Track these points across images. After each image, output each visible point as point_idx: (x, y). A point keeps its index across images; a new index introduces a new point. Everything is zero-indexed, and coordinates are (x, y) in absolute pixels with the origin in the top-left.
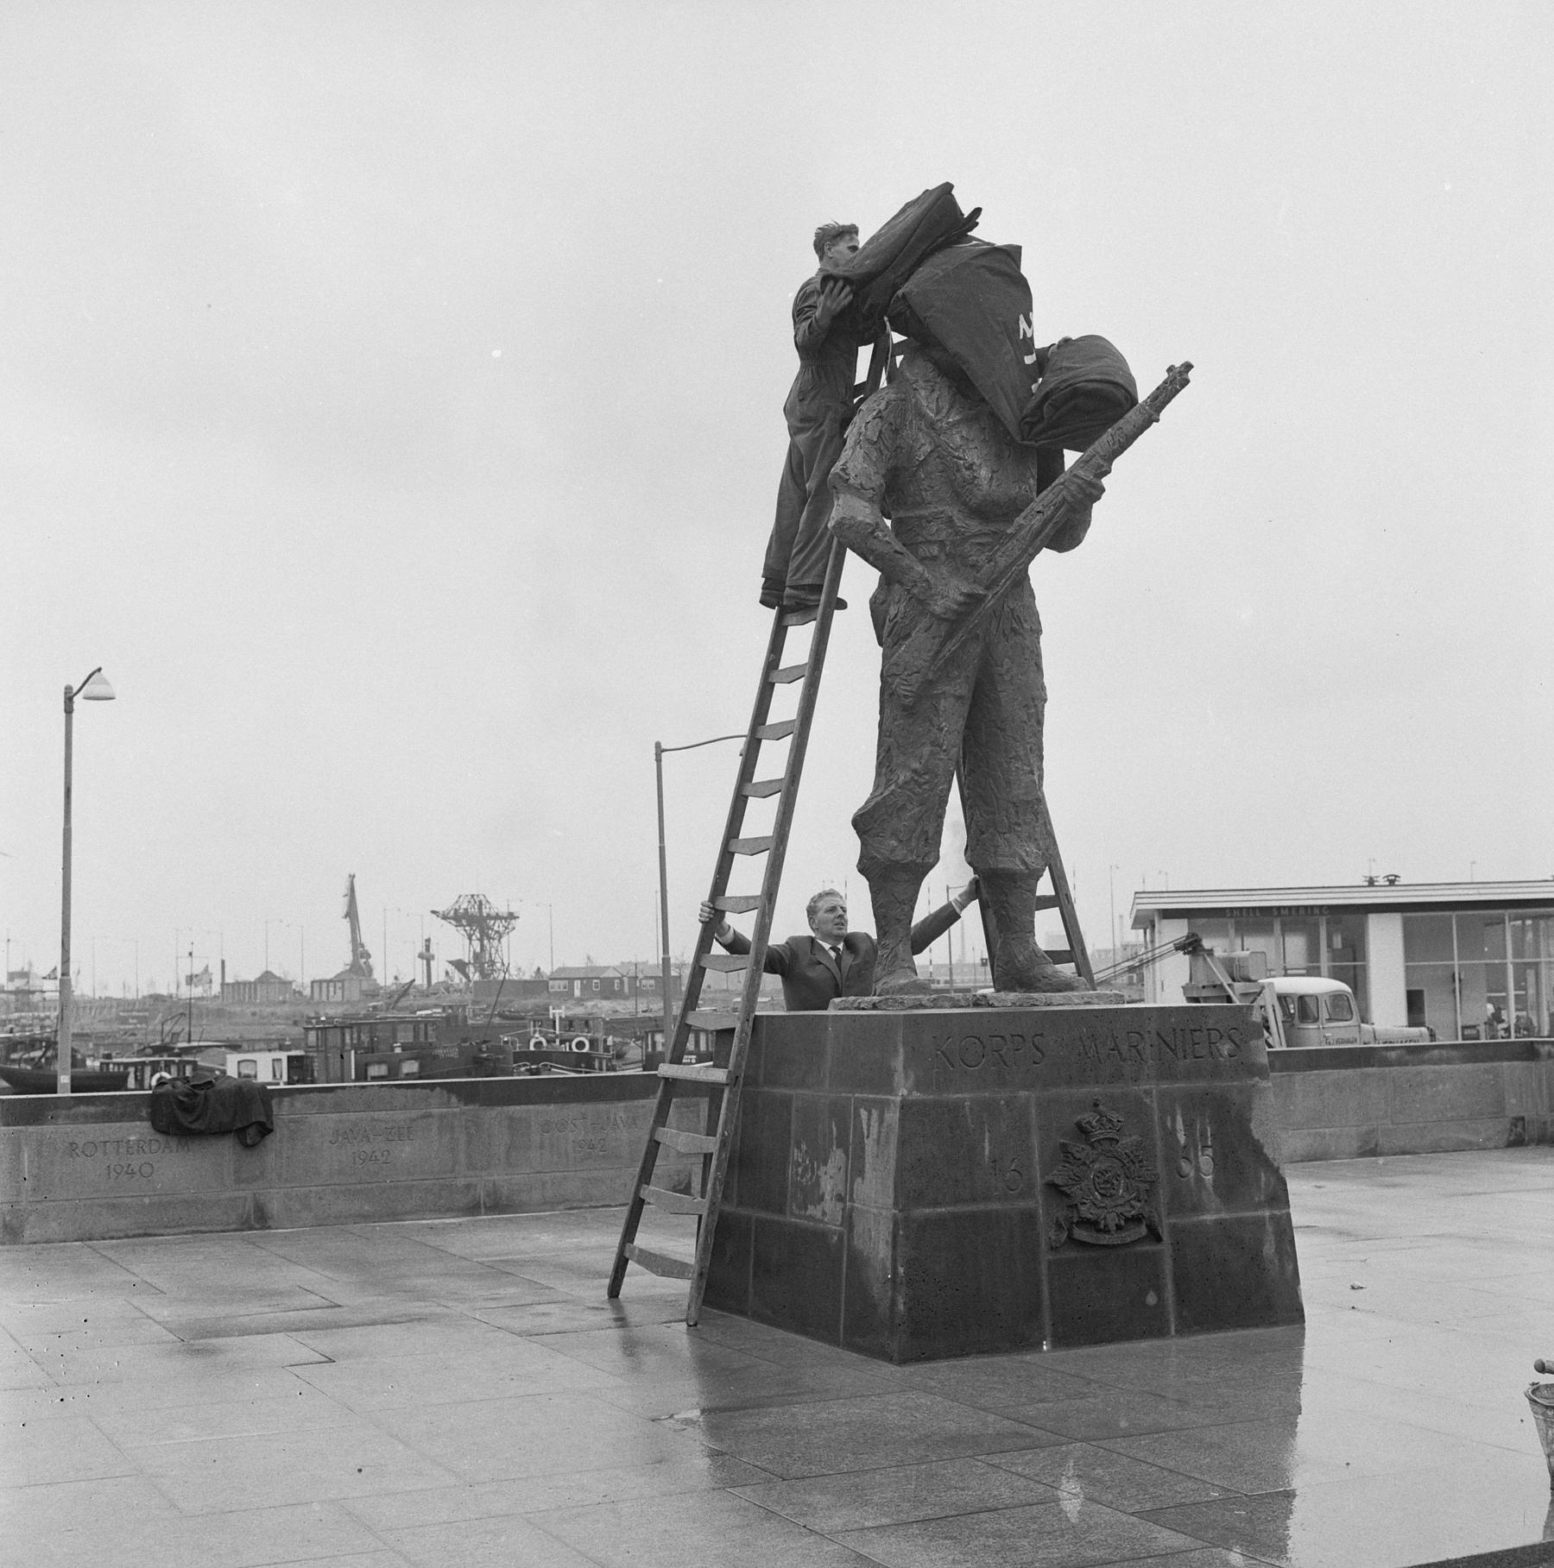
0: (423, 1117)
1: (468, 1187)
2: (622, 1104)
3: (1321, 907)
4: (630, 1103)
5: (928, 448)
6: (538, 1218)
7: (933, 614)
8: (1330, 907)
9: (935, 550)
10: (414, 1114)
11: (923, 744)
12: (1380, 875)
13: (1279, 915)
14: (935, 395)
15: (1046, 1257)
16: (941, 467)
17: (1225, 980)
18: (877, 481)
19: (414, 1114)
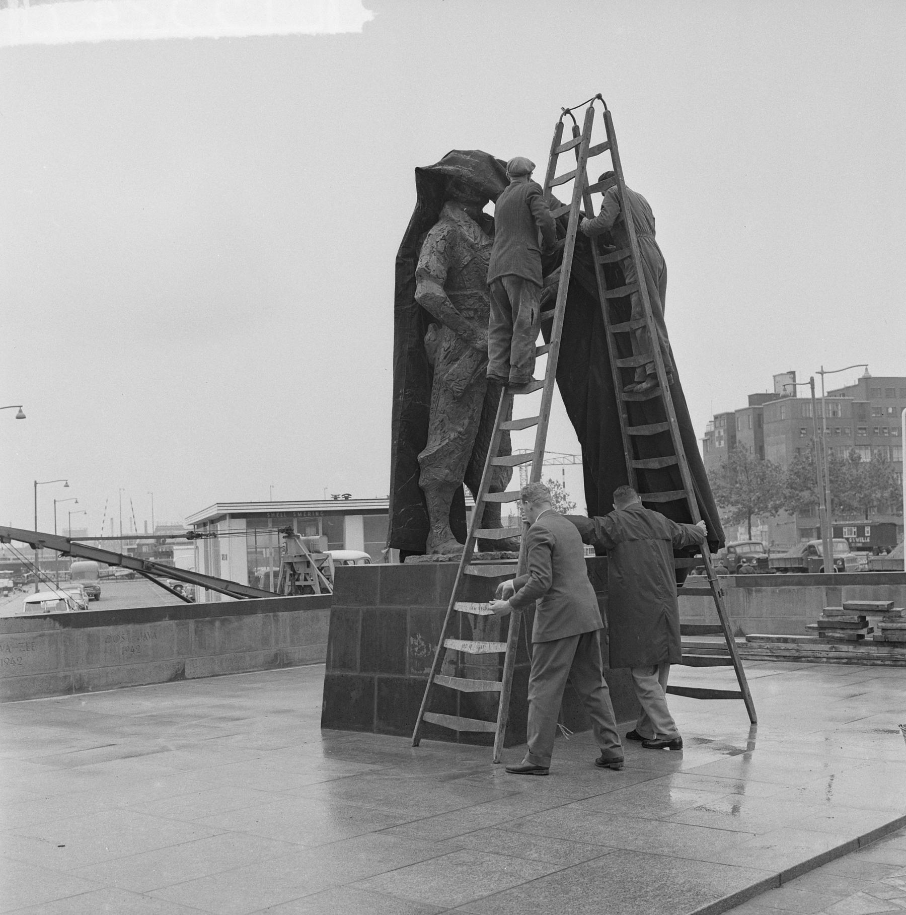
0: (41, 636)
1: (65, 677)
2: (148, 625)
3: (319, 512)
4: (152, 624)
5: (468, 258)
6: (97, 695)
7: (474, 348)
8: (324, 511)
9: (471, 314)
10: (35, 634)
11: (465, 418)
12: (341, 493)
13: (297, 516)
14: (472, 229)
15: (846, 398)
16: (475, 269)
17: (307, 553)
18: (444, 275)
19: (35, 634)
